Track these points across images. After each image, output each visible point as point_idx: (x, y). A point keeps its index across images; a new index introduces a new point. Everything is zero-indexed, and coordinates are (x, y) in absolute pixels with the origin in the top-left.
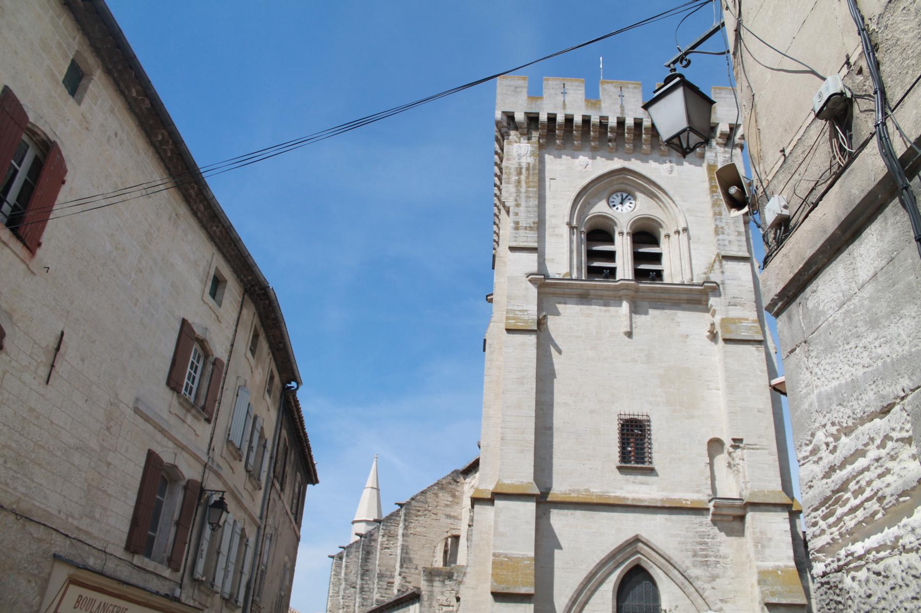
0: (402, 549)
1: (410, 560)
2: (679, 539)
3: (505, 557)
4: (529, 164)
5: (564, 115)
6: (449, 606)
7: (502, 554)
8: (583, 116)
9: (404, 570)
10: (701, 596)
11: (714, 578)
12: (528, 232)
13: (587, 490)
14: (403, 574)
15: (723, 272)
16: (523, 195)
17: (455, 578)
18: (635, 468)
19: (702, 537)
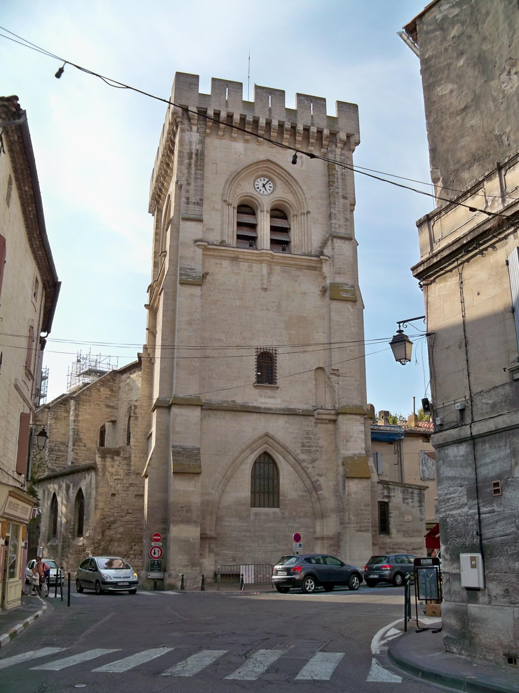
0: (74, 432)
1: (80, 440)
2: (293, 435)
3: (180, 448)
4: (197, 150)
5: (226, 113)
6: (117, 475)
7: (178, 446)
8: (240, 114)
9: (76, 447)
10: (306, 472)
11: (314, 461)
12: (196, 206)
13: (234, 401)
14: (76, 451)
15: (333, 249)
16: (193, 176)
17: (121, 455)
18: (267, 387)
19: (308, 434)
